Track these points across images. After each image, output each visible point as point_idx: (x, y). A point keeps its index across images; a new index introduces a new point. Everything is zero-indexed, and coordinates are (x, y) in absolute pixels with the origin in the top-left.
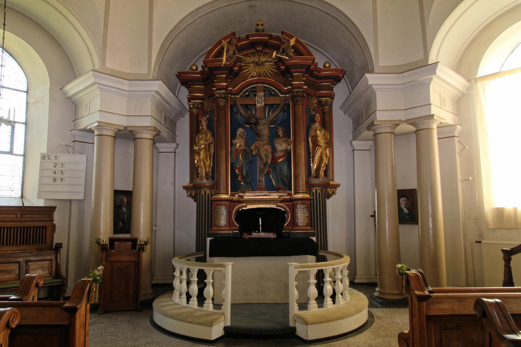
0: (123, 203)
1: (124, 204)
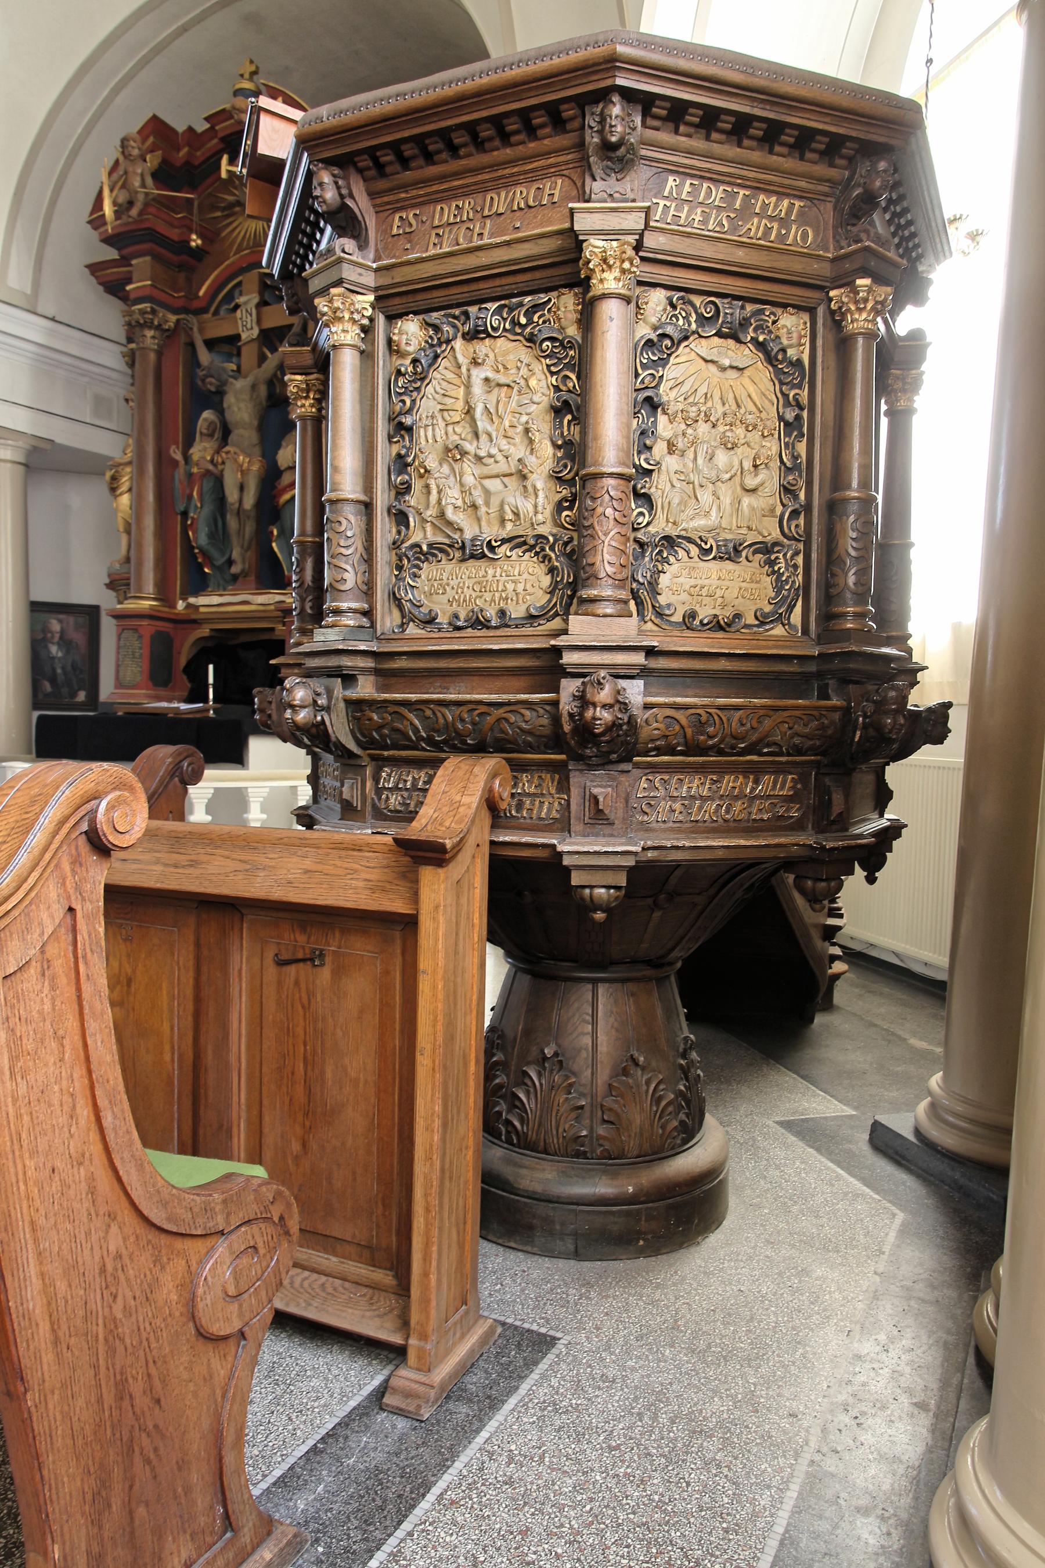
0: (49, 635)
1: (53, 637)
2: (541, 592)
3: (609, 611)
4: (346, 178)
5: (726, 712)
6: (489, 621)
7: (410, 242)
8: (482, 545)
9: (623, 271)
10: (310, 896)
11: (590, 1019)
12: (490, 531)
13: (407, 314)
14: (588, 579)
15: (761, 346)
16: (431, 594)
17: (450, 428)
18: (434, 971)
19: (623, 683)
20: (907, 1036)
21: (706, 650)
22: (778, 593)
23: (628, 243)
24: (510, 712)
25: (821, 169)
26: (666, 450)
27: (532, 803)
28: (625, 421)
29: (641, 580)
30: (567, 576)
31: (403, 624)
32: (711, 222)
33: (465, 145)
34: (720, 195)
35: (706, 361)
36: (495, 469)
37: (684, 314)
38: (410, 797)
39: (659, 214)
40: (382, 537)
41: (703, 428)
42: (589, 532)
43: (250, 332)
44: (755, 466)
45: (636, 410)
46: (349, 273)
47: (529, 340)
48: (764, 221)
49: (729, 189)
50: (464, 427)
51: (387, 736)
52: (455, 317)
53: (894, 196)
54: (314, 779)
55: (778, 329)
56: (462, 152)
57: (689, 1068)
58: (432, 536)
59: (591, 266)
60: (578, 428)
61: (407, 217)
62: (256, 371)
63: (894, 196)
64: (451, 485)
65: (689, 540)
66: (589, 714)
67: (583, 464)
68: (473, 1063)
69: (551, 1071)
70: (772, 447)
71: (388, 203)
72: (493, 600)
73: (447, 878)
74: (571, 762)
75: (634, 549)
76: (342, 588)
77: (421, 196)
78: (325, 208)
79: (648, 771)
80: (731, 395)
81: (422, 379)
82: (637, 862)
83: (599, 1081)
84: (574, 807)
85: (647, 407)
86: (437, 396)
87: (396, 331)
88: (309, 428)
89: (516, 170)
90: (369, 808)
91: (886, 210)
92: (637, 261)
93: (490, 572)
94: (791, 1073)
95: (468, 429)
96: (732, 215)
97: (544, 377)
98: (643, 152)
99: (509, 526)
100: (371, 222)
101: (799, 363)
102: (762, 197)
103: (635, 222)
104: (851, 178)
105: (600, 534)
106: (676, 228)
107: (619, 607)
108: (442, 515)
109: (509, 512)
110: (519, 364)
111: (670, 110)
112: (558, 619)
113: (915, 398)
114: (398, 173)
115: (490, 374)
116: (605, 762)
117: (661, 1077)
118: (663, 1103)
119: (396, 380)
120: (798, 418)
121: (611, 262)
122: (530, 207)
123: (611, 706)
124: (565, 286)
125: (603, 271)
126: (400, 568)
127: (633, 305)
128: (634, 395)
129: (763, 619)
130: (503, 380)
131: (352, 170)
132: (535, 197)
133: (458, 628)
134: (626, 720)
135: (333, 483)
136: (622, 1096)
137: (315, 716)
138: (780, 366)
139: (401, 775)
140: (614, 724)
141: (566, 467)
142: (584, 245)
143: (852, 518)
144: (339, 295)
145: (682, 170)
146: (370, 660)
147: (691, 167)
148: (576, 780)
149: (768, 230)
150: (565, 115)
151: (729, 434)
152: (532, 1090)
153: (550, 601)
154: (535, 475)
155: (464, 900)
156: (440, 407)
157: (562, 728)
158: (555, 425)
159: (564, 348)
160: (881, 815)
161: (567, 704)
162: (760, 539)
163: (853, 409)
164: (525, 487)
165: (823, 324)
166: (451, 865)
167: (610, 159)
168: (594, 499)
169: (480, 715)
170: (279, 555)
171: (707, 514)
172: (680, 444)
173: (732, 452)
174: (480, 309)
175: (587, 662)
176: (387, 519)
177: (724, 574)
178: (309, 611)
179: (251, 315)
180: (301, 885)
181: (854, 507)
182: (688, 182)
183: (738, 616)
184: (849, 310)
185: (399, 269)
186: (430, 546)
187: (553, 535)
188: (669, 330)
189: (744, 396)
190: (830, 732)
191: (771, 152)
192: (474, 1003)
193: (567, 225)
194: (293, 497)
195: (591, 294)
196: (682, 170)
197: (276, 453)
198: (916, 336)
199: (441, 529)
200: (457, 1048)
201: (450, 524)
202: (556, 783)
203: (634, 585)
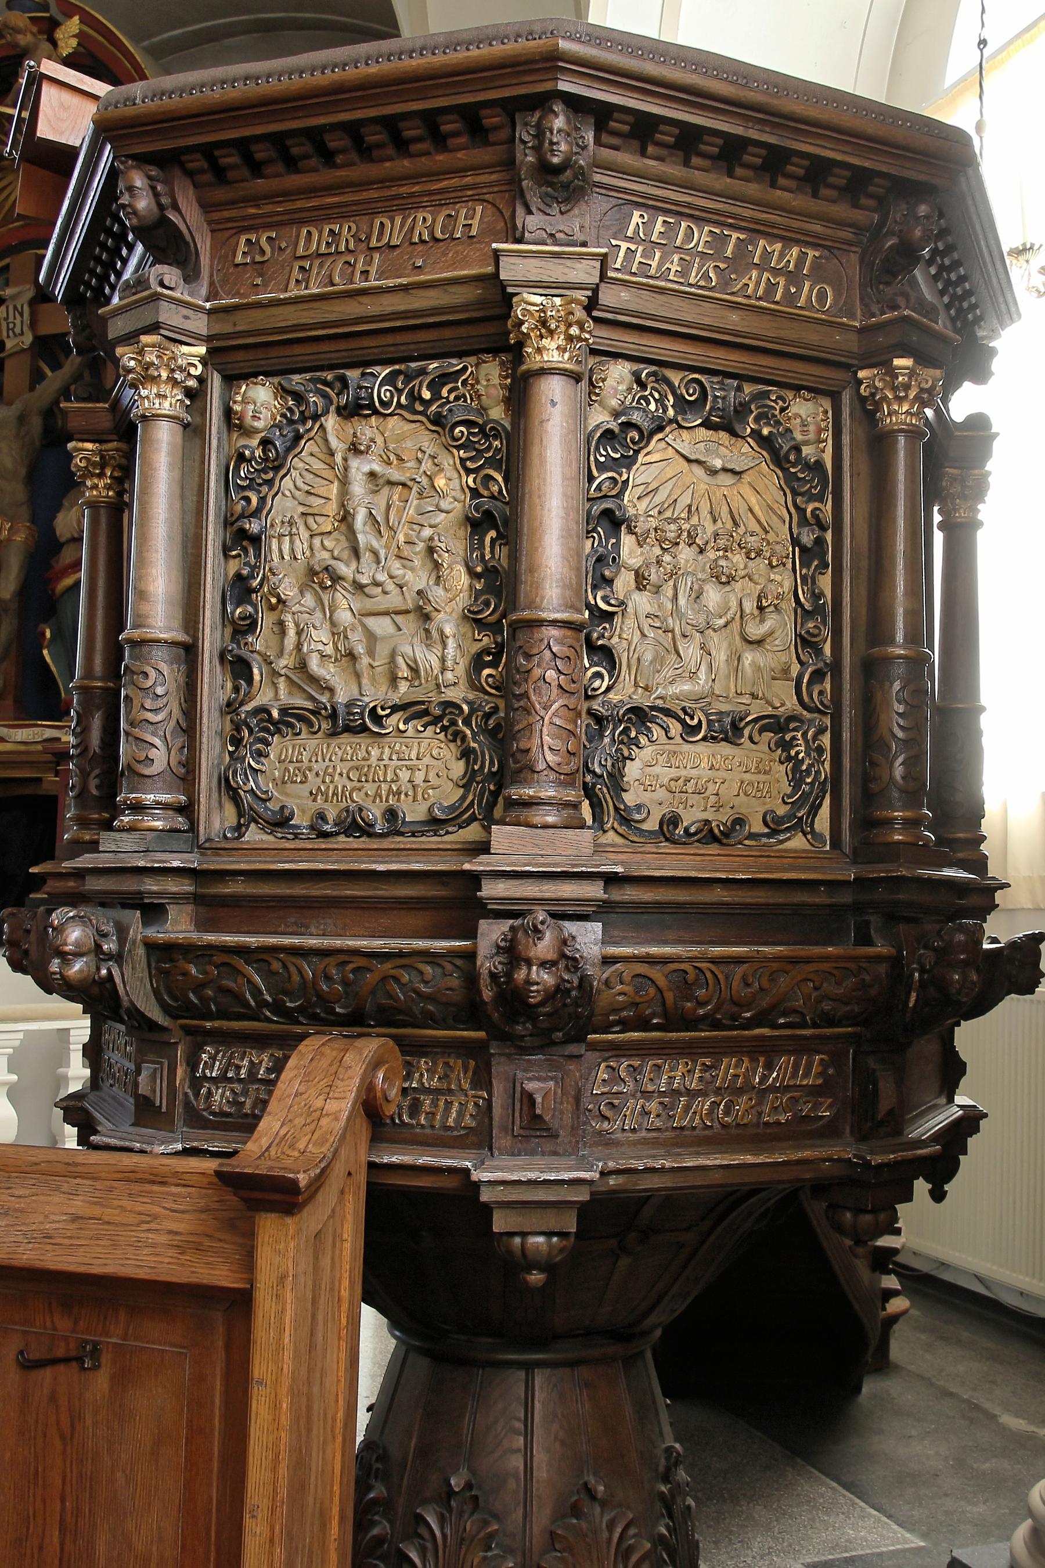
2: (451, 784)
3: (550, 819)
4: (168, 182)
5: (723, 967)
6: (372, 826)
7: (261, 275)
8: (362, 714)
9: (570, 339)
10: (80, 1260)
11: (522, 1426)
12: (375, 694)
13: (256, 375)
14: (520, 771)
15: (766, 443)
16: (284, 782)
17: (317, 541)
18: (276, 1382)
19: (571, 927)
20: (997, 1411)
21: (693, 874)
22: (796, 788)
23: (577, 302)
24: (402, 967)
25: (841, 210)
26: (633, 584)
27: (435, 1104)
28: (573, 546)
29: (598, 770)
30: (489, 763)
31: (239, 826)
32: (693, 274)
33: (342, 151)
34: (704, 238)
35: (689, 461)
36: (382, 602)
37: (657, 396)
38: (245, 1093)
39: (619, 260)
40: (210, 694)
41: (685, 554)
42: (522, 703)
43: (20, 339)
44: (761, 608)
45: (590, 528)
46: (168, 315)
47: (434, 423)
48: (766, 275)
49: (717, 231)
50: (337, 540)
51: (210, 999)
52: (326, 383)
53: (941, 246)
54: (93, 1052)
55: (789, 419)
56: (339, 159)
57: (673, 1497)
58: (286, 696)
59: (524, 329)
60: (505, 550)
61: (258, 240)
62: (27, 395)
63: (941, 246)
64: (318, 625)
65: (668, 713)
66: (521, 975)
67: (513, 604)
68: (335, 1523)
69: (461, 1513)
70: (784, 581)
71: (229, 220)
72: (378, 794)
73: (299, 1231)
74: (494, 1043)
75: (588, 726)
76: (147, 771)
77: (279, 214)
78: (135, 221)
79: (610, 1054)
80: (725, 509)
81: (276, 469)
82: (592, 1194)
83: (535, 1528)
84: (497, 1111)
85: (605, 523)
86: (297, 493)
87: (239, 398)
88: (103, 520)
89: (416, 188)
90: (179, 1109)
91: (930, 262)
92: (590, 324)
93: (375, 752)
94: (828, 1481)
95: (345, 544)
96: (722, 266)
97: (456, 475)
98: (597, 178)
99: (403, 687)
100: (204, 244)
101: (819, 465)
102: (762, 242)
103: (585, 272)
104: (882, 224)
105: (538, 706)
106: (645, 280)
107: (565, 813)
108: (302, 666)
109: (404, 666)
110: (420, 455)
111: (633, 126)
112: (475, 826)
113: (980, 507)
114: (242, 181)
115: (377, 467)
116: (545, 1042)
117: (631, 1516)
118: (634, 1558)
119: (237, 468)
120: (819, 541)
121: (553, 326)
122: (437, 240)
123: (554, 963)
124: (487, 351)
125: (541, 337)
126: (237, 742)
127: (584, 384)
128: (587, 506)
129: (775, 826)
130: (396, 475)
131: (177, 172)
132: (444, 227)
133: (325, 835)
134: (576, 982)
135: (138, 616)
136: (570, 1550)
137: (98, 969)
138: (792, 470)
139: (231, 1057)
140: (558, 989)
141: (487, 604)
142: (515, 299)
143: (897, 685)
144: (154, 346)
145: (651, 203)
146: (186, 881)
147: (664, 200)
148: (501, 1069)
149: (771, 287)
150: (487, 122)
151: (722, 563)
152: (429, 1545)
153: (463, 798)
154: (442, 615)
155: (326, 1262)
156: (301, 509)
157: (481, 996)
158: (472, 545)
159: (486, 436)
160: (951, 1100)
161: (487, 962)
162: (769, 710)
163: (894, 534)
164: (427, 631)
165: (851, 414)
166: (305, 1212)
167: (550, 184)
168: (528, 656)
169: (354, 971)
170: (53, 668)
171: (693, 675)
172: (654, 575)
173: (728, 588)
174: (363, 374)
175: (518, 895)
176: (218, 668)
177: (718, 762)
178: (95, 792)
179: (21, 314)
180: (66, 1241)
181: (899, 670)
182: (661, 219)
183: (739, 821)
184: (885, 398)
185: (244, 312)
186: (283, 711)
187: (468, 703)
188: (636, 417)
189: (743, 509)
190: (873, 992)
191: (773, 185)
192: (339, 1424)
193: (490, 269)
194: (78, 583)
195: (524, 367)
196: (651, 203)
197: (54, 517)
198: (978, 424)
199: (300, 687)
200: (311, 1500)
201: (314, 680)
202: (470, 1073)
203: (588, 778)
